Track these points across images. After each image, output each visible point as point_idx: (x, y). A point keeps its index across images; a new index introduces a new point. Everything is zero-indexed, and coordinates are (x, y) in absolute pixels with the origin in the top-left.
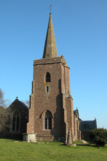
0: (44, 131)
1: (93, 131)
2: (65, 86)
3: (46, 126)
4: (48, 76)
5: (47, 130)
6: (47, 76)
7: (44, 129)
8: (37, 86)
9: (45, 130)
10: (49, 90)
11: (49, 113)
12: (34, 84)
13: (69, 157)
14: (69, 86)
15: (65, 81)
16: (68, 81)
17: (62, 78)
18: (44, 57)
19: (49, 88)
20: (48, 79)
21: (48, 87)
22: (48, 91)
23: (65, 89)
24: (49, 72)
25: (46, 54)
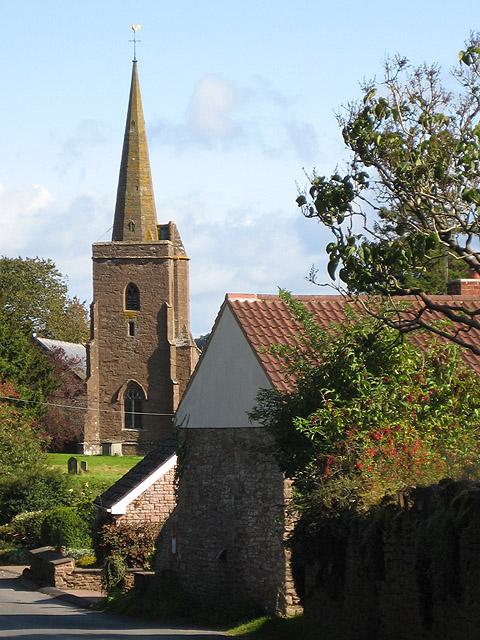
0: (124, 432)
1: (413, 172)
2: (176, 315)
4: (133, 291)
6: (128, 292)
8: (105, 320)
10: (135, 332)
11: (133, 388)
12: (96, 314)
13: (180, 329)
14: (186, 314)
15: (176, 301)
16: (185, 305)
17: (168, 301)
18: (118, 232)
19: (136, 326)
20: (133, 302)
21: (132, 324)
22: (132, 333)
23: (177, 323)
24: (135, 282)
25: (126, 222)
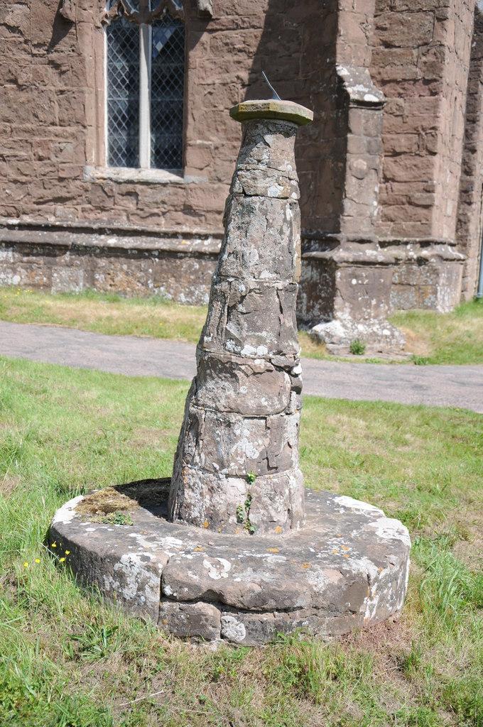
0: (103, 193)
3: (126, 120)
5: (127, 173)
7: (101, 168)
9: (107, 171)
